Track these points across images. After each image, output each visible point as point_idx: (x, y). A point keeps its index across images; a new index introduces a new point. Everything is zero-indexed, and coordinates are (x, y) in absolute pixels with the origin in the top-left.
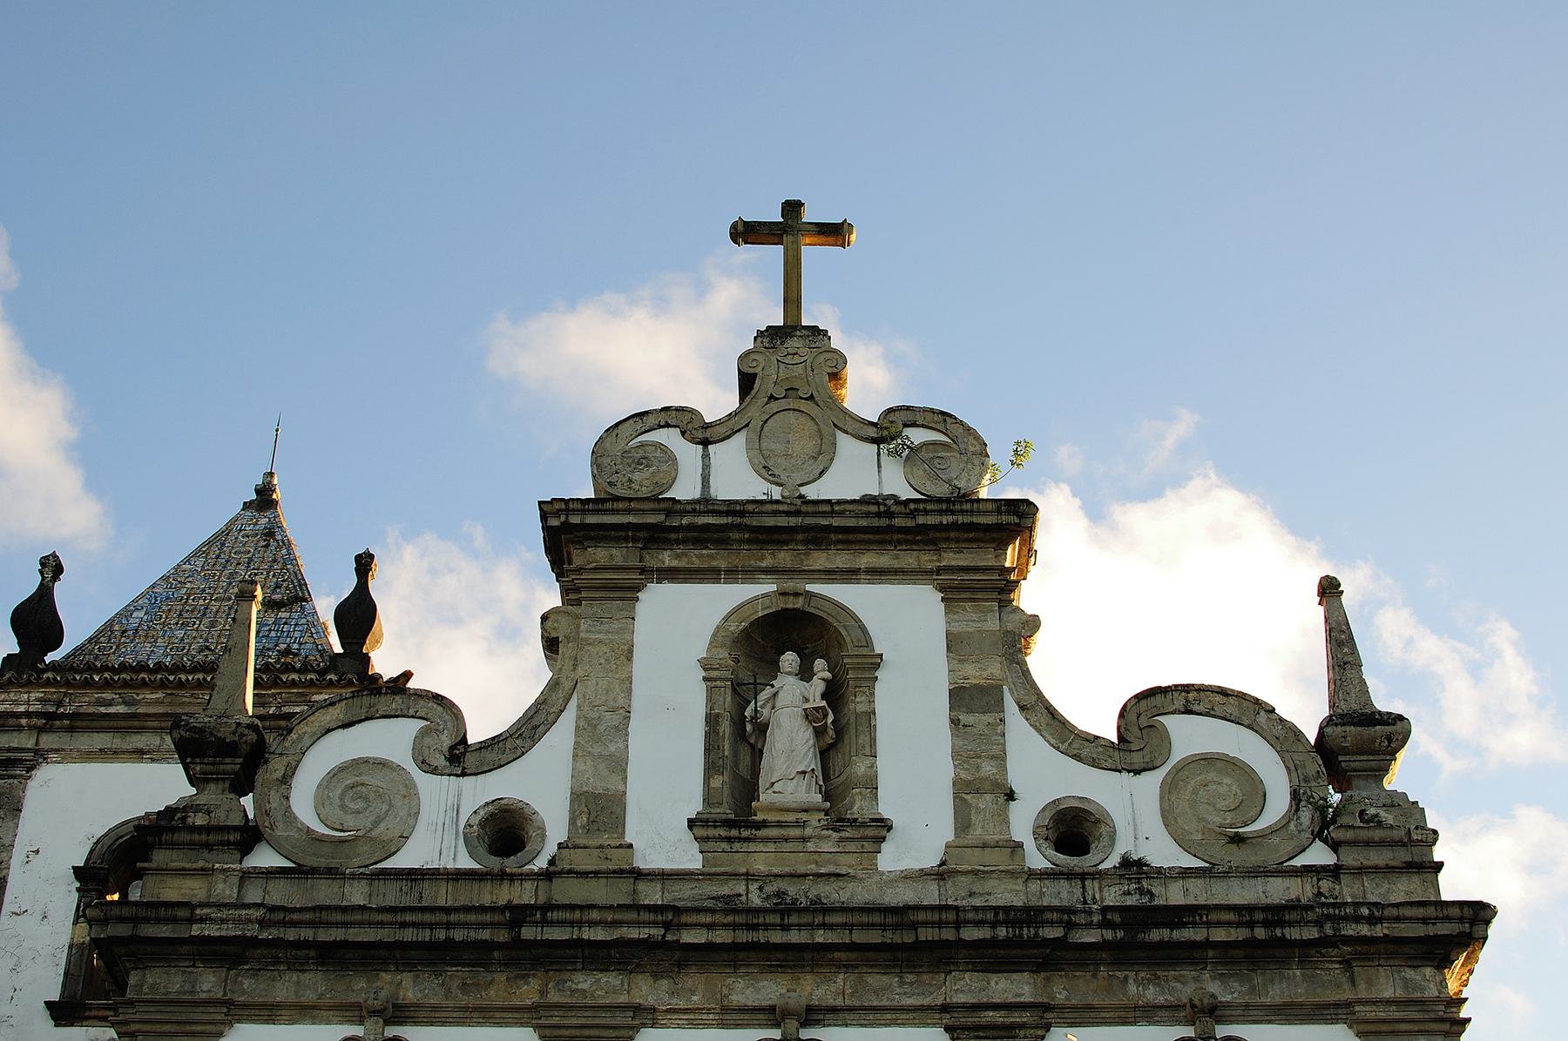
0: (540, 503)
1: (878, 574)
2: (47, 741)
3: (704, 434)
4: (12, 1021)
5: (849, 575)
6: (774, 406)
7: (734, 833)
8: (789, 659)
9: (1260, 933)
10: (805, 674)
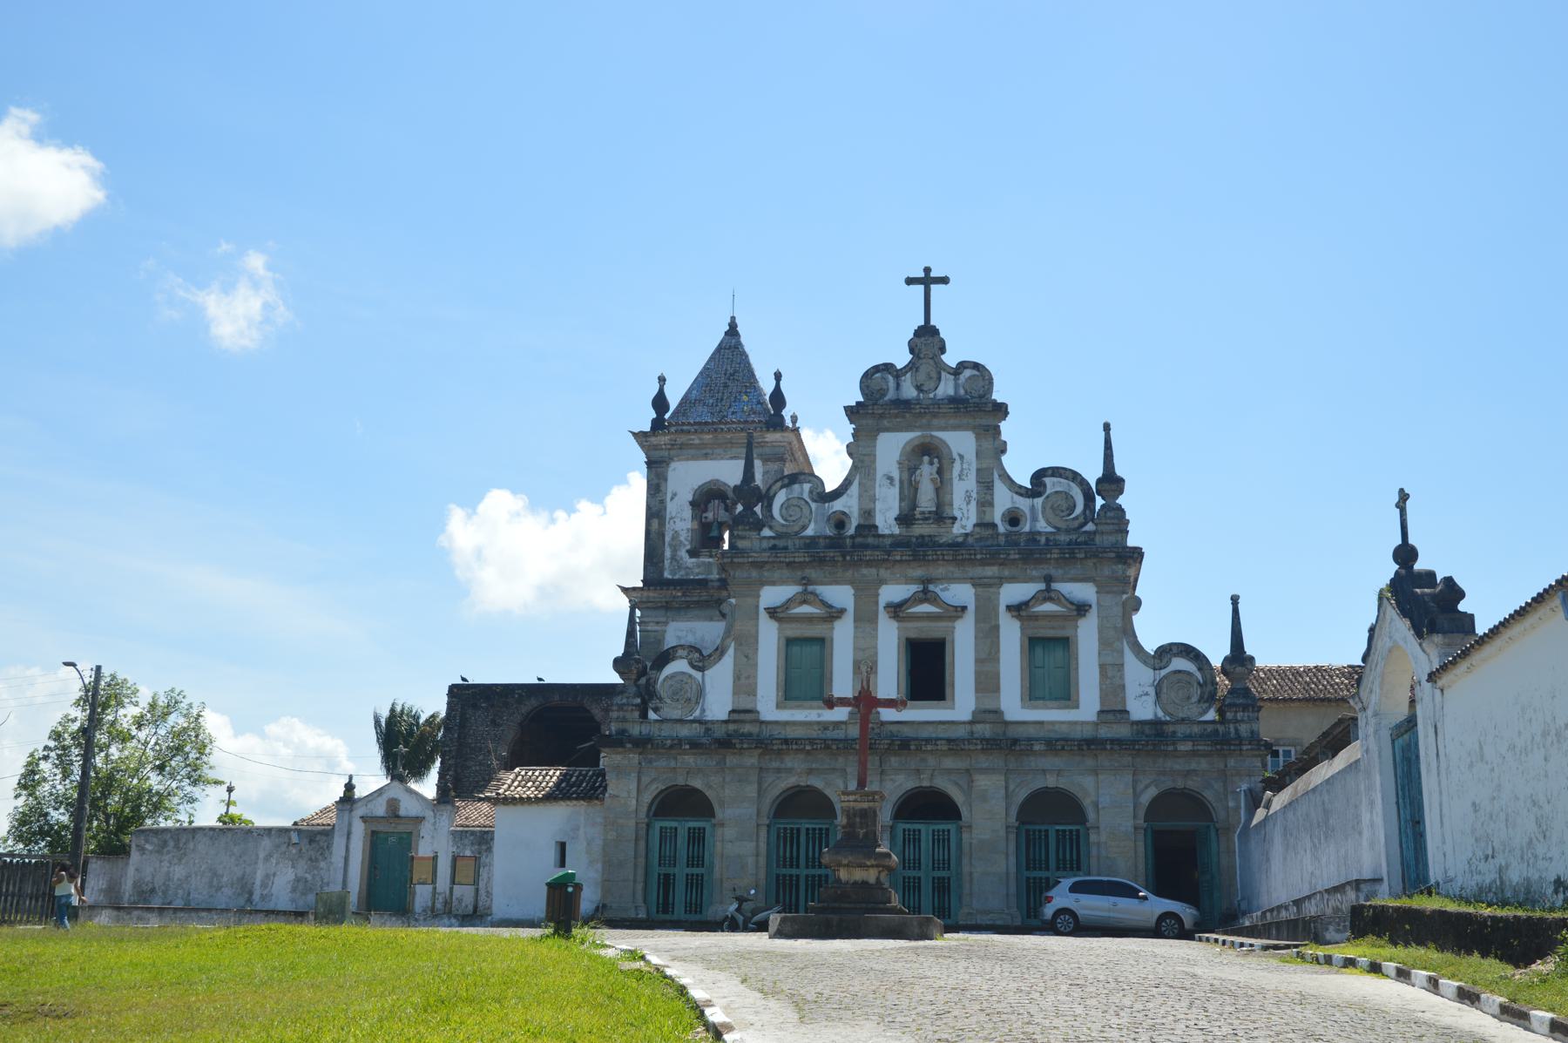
2: (672, 452)
3: (898, 374)
10: (931, 463)
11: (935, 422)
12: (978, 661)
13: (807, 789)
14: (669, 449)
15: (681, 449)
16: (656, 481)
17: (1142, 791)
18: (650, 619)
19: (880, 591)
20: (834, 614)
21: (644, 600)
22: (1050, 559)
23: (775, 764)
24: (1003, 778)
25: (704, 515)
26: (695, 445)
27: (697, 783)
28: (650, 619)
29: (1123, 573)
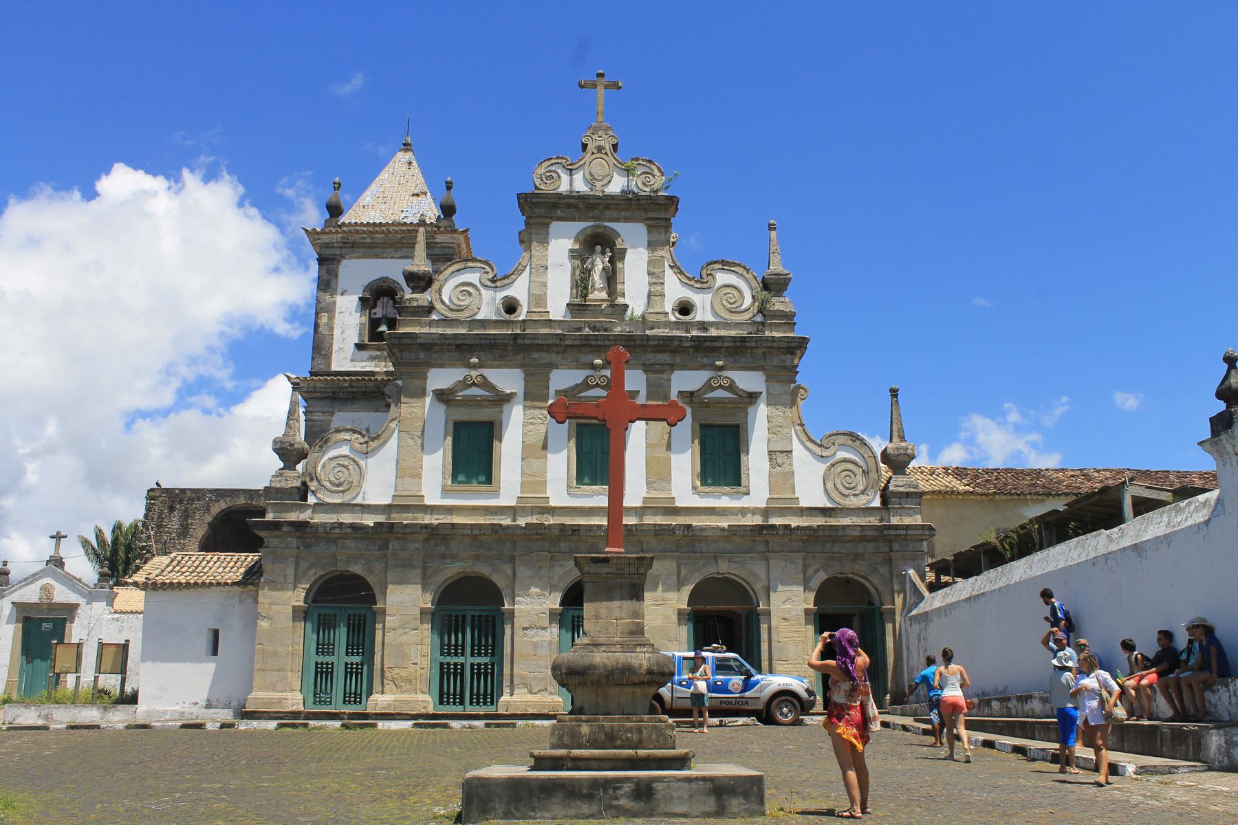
0: (518, 194)
1: (626, 220)
2: (344, 251)
4: (344, 350)
5: (617, 220)
6: (594, 156)
7: (581, 308)
8: (598, 248)
9: (738, 344)
10: (603, 253)
11: (608, 213)
12: (1062, 537)
13: (473, 575)
14: (341, 247)
15: (352, 247)
16: (326, 277)
17: (811, 578)
18: (317, 409)
19: (551, 376)
20: (503, 399)
21: (311, 390)
22: (721, 347)
23: (441, 549)
24: (674, 564)
25: (373, 311)
26: (368, 243)
27: (357, 569)
28: (317, 409)
29: (791, 363)
